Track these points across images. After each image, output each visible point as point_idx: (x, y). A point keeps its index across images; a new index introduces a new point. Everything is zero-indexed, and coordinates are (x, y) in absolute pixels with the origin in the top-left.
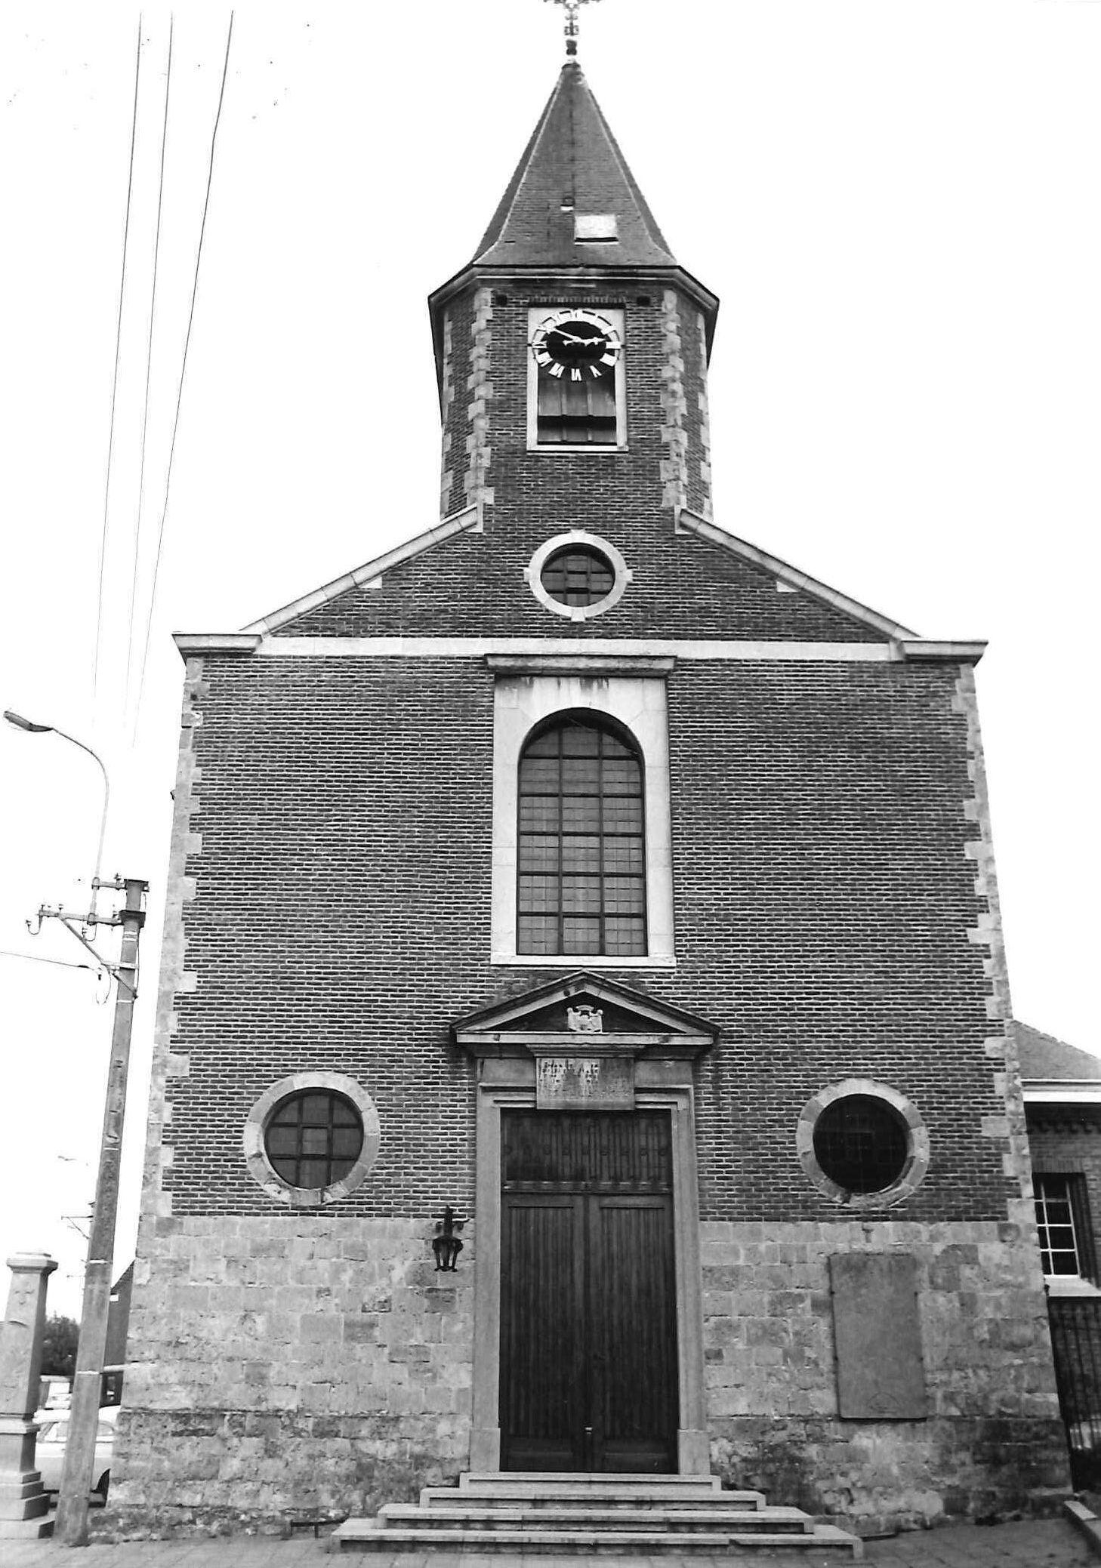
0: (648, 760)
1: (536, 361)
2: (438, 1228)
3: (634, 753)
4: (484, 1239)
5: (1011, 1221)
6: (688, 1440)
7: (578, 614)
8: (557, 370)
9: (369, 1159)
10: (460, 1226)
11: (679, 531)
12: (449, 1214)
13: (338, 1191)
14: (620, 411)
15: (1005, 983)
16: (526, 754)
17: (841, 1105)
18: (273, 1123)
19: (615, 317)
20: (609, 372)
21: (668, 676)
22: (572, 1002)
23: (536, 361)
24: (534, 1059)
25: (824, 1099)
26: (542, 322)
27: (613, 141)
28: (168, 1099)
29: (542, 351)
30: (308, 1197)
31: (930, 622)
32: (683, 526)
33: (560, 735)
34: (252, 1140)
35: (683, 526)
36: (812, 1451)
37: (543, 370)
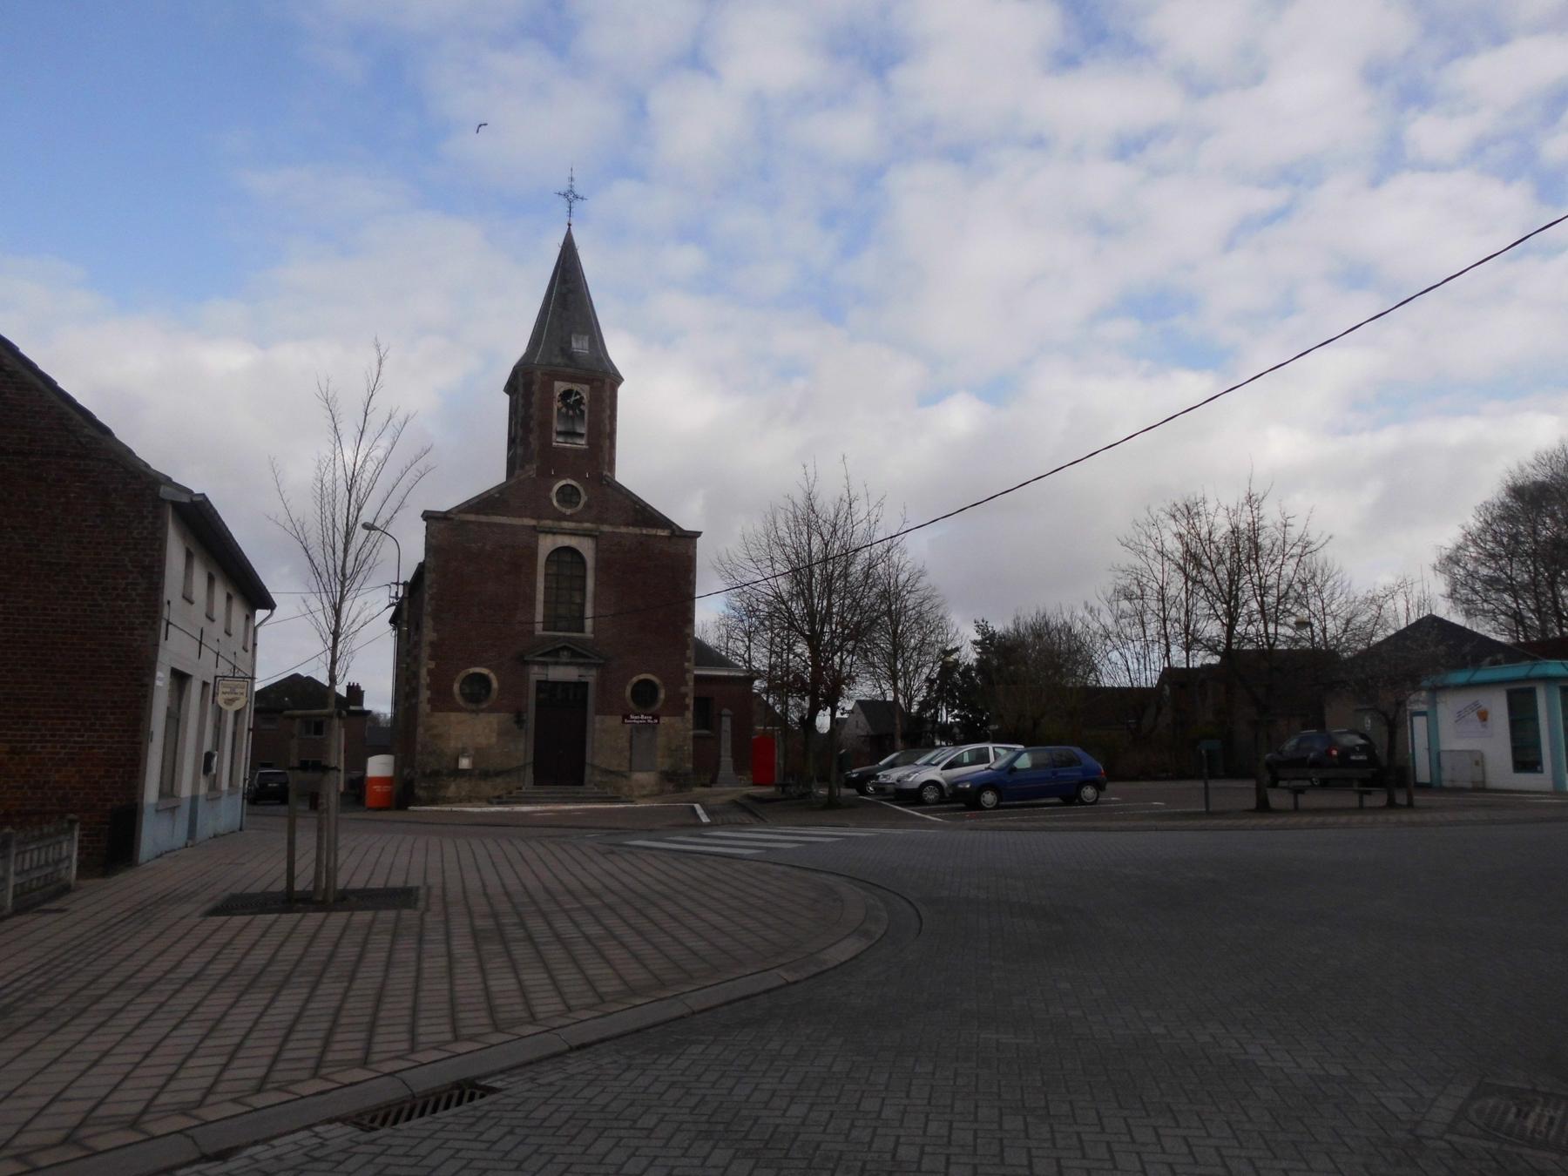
1: (557, 405)
4: (531, 716)
7: (569, 512)
9: (494, 695)
13: (484, 706)
14: (12, 881)
15: (476, 712)
16: (548, 559)
17: (640, 682)
18: (463, 682)
19: (587, 387)
20: (582, 412)
22: (564, 648)
23: (557, 405)
25: (635, 679)
26: (560, 387)
27: (255, 645)
30: (474, 707)
31: (687, 525)
36: (36, 833)
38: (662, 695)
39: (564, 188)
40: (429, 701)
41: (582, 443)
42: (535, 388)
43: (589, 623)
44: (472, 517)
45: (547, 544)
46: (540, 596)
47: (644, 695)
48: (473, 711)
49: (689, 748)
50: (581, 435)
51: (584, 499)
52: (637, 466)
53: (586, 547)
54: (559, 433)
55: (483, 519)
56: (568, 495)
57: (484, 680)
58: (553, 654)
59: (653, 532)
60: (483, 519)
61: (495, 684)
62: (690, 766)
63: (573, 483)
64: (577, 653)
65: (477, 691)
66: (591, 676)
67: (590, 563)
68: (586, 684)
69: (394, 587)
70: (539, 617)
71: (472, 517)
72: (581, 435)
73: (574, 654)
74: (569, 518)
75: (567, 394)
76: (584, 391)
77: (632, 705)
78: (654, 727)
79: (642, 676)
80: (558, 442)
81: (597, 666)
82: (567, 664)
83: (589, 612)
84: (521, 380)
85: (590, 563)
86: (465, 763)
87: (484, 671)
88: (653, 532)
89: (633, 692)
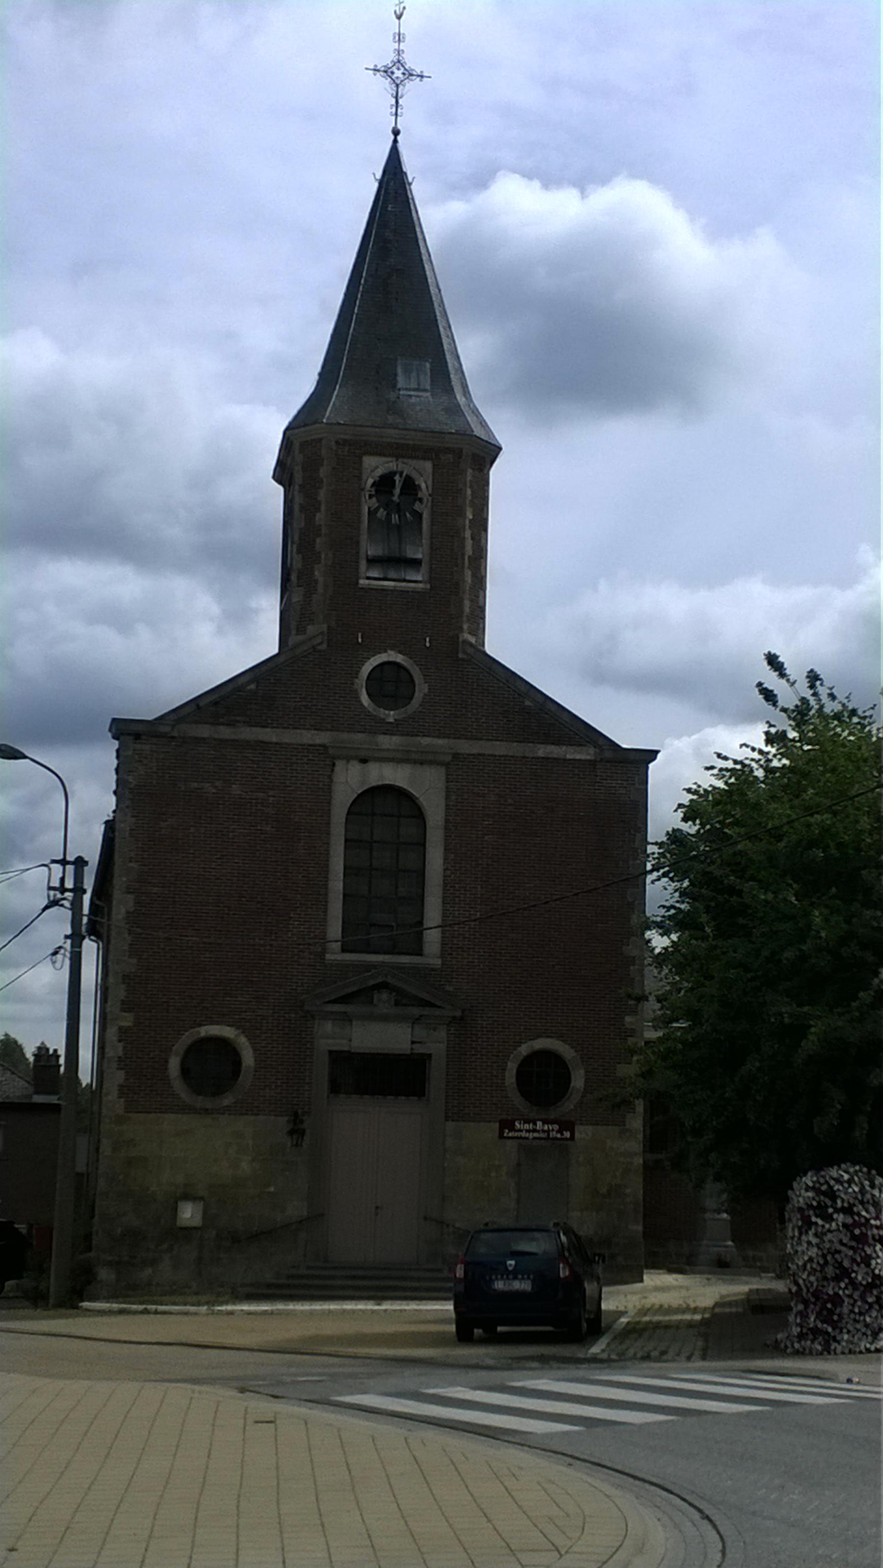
0: (430, 823)
2: (288, 1121)
3: (418, 814)
5: (627, 1126)
6: (419, 1049)
7: (391, 716)
8: (382, 513)
9: (246, 1079)
10: (302, 1122)
11: (461, 656)
12: (296, 1114)
13: (227, 1100)
19: (428, 465)
20: (419, 516)
21: (454, 764)
24: (351, 1021)
25: (524, 1050)
26: (374, 466)
28: (120, 1041)
29: (371, 496)
30: (200, 1102)
32: (465, 653)
33: (70, 909)
34: (174, 1064)
35: (465, 653)
37: (372, 513)
38: (578, 1081)
39: (388, 59)
40: (123, 1090)
41: (417, 580)
42: (323, 472)
43: (432, 938)
44: (204, 731)
45: (350, 781)
46: (337, 885)
47: (543, 1080)
48: (206, 1111)
49: (635, 1188)
50: (415, 563)
51: (421, 689)
52: (524, 626)
53: (428, 787)
54: (372, 561)
55: (225, 733)
56: (390, 685)
57: (225, 1049)
58: (359, 996)
59: (555, 751)
60: (225, 733)
61: (248, 1058)
62: (638, 1228)
63: (399, 658)
64: (410, 997)
65: (212, 1069)
66: (436, 1044)
67: (435, 814)
68: (425, 1059)
69: (57, 869)
70: (335, 929)
71: (204, 731)
72: (415, 563)
73: (402, 999)
74: (390, 729)
75: (385, 483)
76: (423, 474)
77: (517, 1100)
78: (413, 1042)
79: (540, 1044)
80: (370, 578)
81: (176, 1203)
82: (385, 1018)
83: (433, 914)
84: (299, 458)
85: (435, 814)
86: (189, 1214)
87: (227, 1032)
88: (555, 751)
89: (520, 1074)
